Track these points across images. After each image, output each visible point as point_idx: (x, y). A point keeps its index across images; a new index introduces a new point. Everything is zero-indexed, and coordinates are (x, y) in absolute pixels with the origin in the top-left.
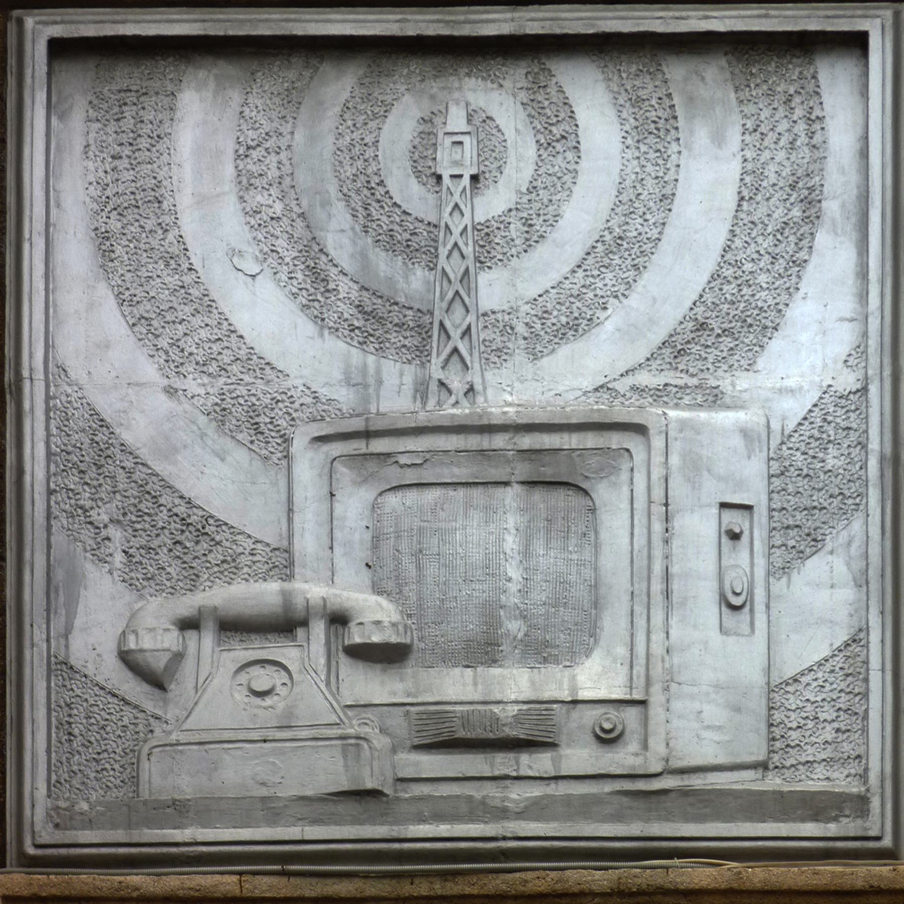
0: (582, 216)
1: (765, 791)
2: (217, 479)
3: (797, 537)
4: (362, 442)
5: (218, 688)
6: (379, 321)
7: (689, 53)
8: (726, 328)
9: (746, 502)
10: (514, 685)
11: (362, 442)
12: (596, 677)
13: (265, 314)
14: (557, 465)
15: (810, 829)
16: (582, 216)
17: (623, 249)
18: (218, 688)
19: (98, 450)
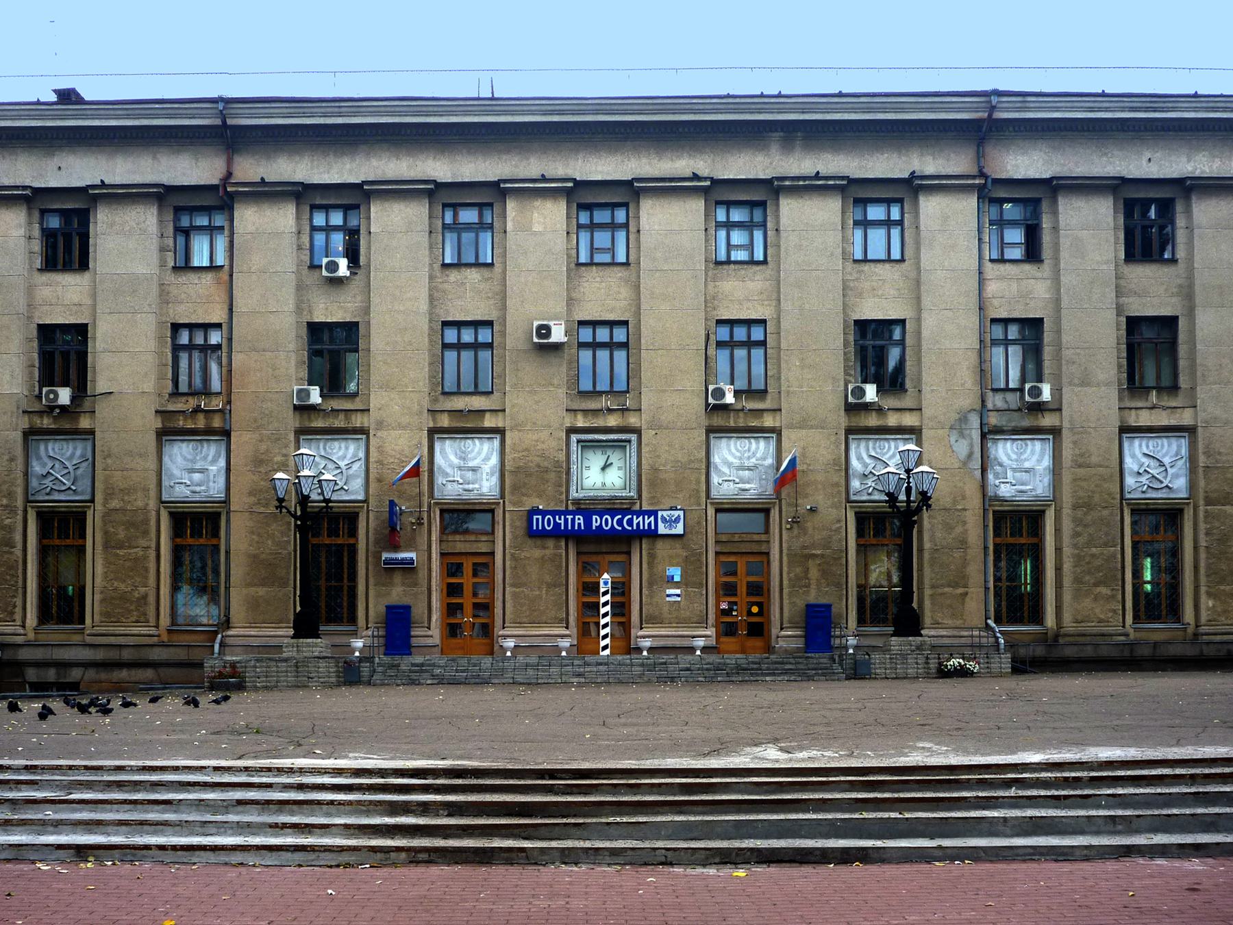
0: (476, 450)
1: (304, 757)
2: (449, 470)
3: (492, 475)
4: (460, 468)
5: (449, 486)
6: (461, 458)
7: (469, 153)
8: (487, 459)
9: (486, 318)
10: (471, 486)
11: (460, 468)
12: (477, 486)
13: (452, 458)
14: (474, 470)
15: (1120, 791)
16: (476, 450)
17: (479, 453)
18: (449, 486)
19: (440, 468)
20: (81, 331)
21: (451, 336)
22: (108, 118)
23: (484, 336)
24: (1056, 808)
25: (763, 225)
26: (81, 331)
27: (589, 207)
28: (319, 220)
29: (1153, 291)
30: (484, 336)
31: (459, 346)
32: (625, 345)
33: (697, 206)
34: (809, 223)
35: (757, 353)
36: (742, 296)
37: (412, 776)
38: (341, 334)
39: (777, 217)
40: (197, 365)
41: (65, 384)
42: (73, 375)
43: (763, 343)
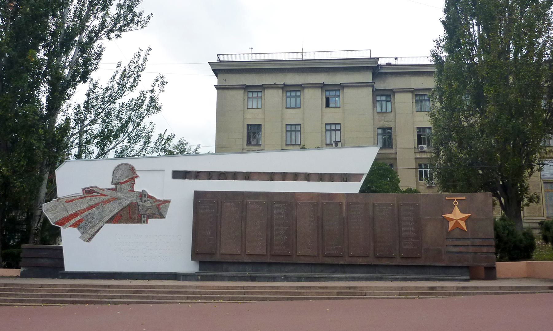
20: (259, 127)
21: (328, 128)
22: (401, 69)
23: (338, 127)
24: (373, 273)
25: (390, 101)
26: (259, 127)
27: (416, 95)
28: (288, 94)
29: (332, 115)
30: (338, 127)
31: (331, 130)
32: (340, 130)
33: (242, 92)
34: (273, 97)
35: (338, 133)
36: (292, 116)
37: (467, 293)
38: (256, 127)
39: (394, 99)
40: (293, 137)
41: (424, 144)
42: (427, 143)
43: (340, 130)
